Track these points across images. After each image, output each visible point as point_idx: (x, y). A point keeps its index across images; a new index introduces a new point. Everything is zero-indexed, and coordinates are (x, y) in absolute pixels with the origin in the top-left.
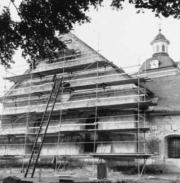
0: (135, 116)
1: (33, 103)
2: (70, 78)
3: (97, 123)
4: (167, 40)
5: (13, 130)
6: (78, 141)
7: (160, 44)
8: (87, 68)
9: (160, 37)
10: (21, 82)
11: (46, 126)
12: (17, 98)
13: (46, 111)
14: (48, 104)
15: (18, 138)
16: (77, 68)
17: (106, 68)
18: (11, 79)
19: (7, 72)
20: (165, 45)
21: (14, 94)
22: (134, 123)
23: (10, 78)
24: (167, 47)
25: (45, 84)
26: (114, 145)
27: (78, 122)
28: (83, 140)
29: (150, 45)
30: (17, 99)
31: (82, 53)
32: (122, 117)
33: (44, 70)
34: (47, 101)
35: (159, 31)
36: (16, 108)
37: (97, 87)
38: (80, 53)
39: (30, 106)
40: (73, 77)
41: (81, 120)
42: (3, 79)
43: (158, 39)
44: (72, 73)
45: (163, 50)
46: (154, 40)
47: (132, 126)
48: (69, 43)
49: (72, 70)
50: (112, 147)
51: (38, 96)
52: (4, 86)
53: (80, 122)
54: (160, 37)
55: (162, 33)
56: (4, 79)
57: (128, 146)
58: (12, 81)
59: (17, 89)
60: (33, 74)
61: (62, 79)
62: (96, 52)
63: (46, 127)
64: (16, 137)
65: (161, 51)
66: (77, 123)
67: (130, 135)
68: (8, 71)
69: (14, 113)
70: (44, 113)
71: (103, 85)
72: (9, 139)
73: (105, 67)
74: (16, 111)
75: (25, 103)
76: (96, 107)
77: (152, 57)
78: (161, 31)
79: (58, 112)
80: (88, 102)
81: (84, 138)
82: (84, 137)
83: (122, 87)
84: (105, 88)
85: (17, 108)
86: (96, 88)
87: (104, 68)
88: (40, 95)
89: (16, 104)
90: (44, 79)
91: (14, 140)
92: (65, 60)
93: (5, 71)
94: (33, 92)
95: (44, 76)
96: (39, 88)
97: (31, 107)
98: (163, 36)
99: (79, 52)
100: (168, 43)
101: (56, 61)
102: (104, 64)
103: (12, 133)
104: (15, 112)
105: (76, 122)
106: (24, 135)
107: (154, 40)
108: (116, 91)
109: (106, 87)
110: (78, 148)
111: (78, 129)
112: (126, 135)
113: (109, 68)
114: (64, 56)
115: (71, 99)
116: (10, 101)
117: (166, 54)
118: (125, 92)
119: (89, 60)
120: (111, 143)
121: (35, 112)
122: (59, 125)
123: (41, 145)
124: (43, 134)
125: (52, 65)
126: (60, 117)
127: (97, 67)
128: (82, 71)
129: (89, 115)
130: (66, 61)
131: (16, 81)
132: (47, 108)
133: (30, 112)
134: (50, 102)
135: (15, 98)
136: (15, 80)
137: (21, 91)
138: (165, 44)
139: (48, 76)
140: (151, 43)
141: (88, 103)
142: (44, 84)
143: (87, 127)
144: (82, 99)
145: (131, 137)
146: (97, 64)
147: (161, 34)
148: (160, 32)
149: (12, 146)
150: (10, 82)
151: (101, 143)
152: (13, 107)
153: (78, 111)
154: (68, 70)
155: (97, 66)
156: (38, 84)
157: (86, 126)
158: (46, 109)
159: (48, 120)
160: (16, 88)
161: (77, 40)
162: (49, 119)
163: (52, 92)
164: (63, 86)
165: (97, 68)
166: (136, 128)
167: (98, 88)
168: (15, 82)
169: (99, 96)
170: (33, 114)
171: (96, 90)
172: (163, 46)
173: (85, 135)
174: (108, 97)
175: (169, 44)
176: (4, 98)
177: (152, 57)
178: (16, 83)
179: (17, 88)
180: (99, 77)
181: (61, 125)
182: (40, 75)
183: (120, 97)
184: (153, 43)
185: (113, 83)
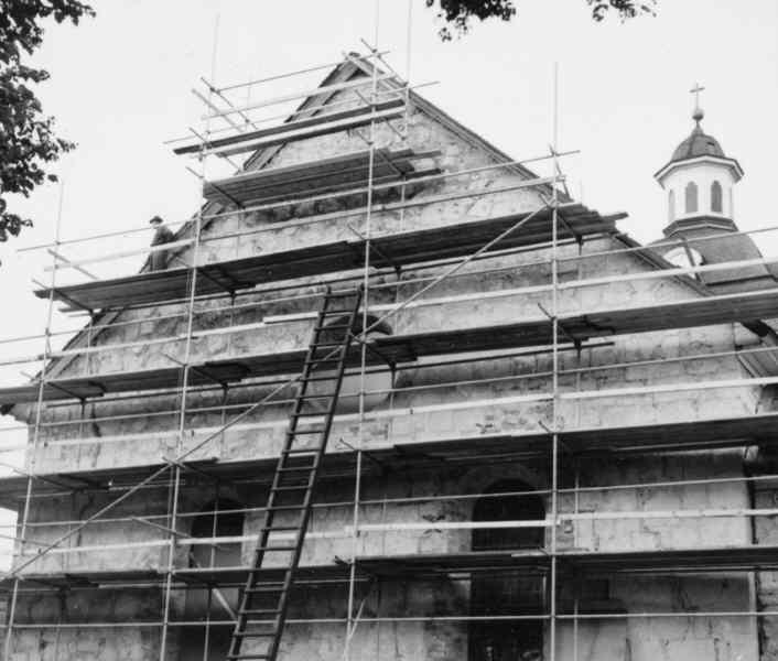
0: (744, 486)
1: (200, 413)
2: (388, 294)
3: (565, 517)
4: (736, 161)
5: (80, 553)
7: (703, 176)
9: (698, 148)
10: (120, 312)
11: (295, 529)
12: (105, 390)
13: (286, 454)
14: (296, 418)
17: (586, 244)
18: (74, 297)
20: (722, 184)
22: (744, 519)
24: (731, 190)
25: (266, 319)
27: (435, 514)
28: (460, 608)
29: (655, 180)
31: (447, 171)
32: (679, 491)
33: (247, 252)
35: (694, 122)
36: (93, 440)
37: (555, 337)
38: (437, 171)
40: (425, 284)
41: (450, 502)
43: (690, 156)
44: (398, 271)
46: (674, 161)
47: (738, 538)
49: (405, 251)
51: (219, 385)
53: (448, 516)
54: (698, 148)
55: (708, 128)
56: (42, 294)
57: (717, 640)
58: (77, 306)
59: (99, 348)
60: (200, 270)
62: (519, 165)
64: (101, 587)
65: (704, 209)
66: (430, 519)
68: (62, 259)
69: (86, 465)
72: (62, 598)
73: (580, 241)
74: (99, 457)
75: (152, 418)
76: (555, 438)
77: (662, 236)
78: (701, 123)
79: (346, 460)
80: (490, 413)
81: (468, 595)
82: (468, 589)
83: (671, 338)
84: (584, 343)
87: (576, 246)
89: (97, 420)
90: (247, 300)
91: (92, 604)
92: (374, 201)
95: (252, 285)
96: (219, 344)
97: (193, 433)
98: (712, 143)
99: (431, 168)
100: (736, 172)
101: (288, 215)
102: (578, 223)
103: (77, 567)
104: (94, 465)
105: (424, 517)
108: (639, 355)
109: (586, 339)
111: (439, 547)
113: (595, 246)
114: (367, 185)
115: (396, 397)
116: (67, 408)
117: (728, 222)
118: (688, 363)
119: (484, 208)
122: (349, 529)
124: (246, 573)
126: (752, 481)
128: (467, 258)
129: (492, 481)
130: (379, 207)
131: (97, 311)
133: (189, 459)
134: (302, 412)
135: (96, 390)
136: (92, 303)
137: (117, 359)
138: (723, 177)
139: (267, 286)
140: (656, 176)
141: (489, 418)
142: (261, 320)
143: (479, 538)
144: (451, 402)
145: (733, 593)
147: (703, 135)
148: (698, 126)
150: (64, 311)
151: (572, 620)
152: (85, 436)
154: (392, 253)
155: (551, 230)
157: (475, 532)
158: (289, 444)
161: (421, 111)
163: (312, 358)
165: (554, 242)
166: (751, 546)
167: (367, 365)
168: (91, 311)
169: (194, 420)
170: (202, 474)
172: (716, 188)
173: (469, 582)
175: (740, 182)
177: (662, 236)
178: (96, 319)
179: (103, 343)
180: (562, 286)
181: (364, 527)
184: (666, 175)
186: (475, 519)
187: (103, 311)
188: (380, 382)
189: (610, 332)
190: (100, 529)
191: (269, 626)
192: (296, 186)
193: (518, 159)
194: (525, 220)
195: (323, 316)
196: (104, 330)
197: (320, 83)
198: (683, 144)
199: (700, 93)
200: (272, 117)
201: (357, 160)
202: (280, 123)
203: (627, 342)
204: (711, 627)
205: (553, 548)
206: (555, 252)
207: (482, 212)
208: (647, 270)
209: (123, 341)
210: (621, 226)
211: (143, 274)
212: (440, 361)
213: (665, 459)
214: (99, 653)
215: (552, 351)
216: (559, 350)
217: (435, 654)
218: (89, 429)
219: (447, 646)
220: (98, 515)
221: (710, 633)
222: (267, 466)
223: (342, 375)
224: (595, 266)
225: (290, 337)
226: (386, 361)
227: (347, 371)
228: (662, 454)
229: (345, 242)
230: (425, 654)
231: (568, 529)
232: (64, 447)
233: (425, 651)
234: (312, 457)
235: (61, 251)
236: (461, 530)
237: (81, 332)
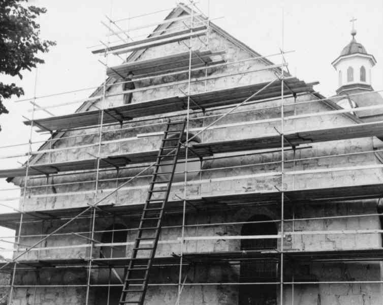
0: (378, 219)
1: (105, 182)
2: (199, 123)
3: (288, 233)
6: (225, 279)
7: (356, 64)
8: (252, 96)
9: (354, 50)
10: (66, 132)
13: (148, 202)
14: (153, 184)
15: (60, 270)
16: (208, 98)
18: (42, 125)
19: (35, 107)
20: (365, 66)
21: (48, 162)
23: (41, 120)
25: (138, 135)
26: (324, 291)
29: (332, 66)
30: (59, 173)
34: (151, 177)
35: (352, 36)
36: (53, 195)
37: (283, 144)
38: (223, 61)
39: (100, 191)
42: (23, 124)
43: (349, 53)
44: (204, 112)
45: (363, 78)
46: (340, 57)
48: (198, 36)
49: (207, 102)
50: (319, 295)
51: (115, 168)
52: (28, 142)
53: (229, 233)
54: (354, 50)
55: (358, 39)
56: (27, 123)
59: (55, 150)
60: (105, 110)
61: (185, 123)
62: (264, 58)
63: (133, 243)
64: (57, 267)
67: (368, 267)
70: (145, 207)
71: (294, 140)
75: (82, 185)
77: (336, 94)
78: (355, 37)
79: (178, 205)
80: (250, 182)
83: (340, 145)
84: (297, 147)
85: (57, 195)
86: (281, 146)
88: (121, 165)
89: (54, 185)
93: (31, 104)
94: (105, 155)
96: (115, 148)
100: (373, 61)
101: (160, 82)
102: (294, 87)
103: (45, 258)
104: (53, 207)
105: (217, 233)
106: (82, 262)
107: (343, 56)
108: (325, 153)
109: (298, 145)
110: (213, 295)
111: (224, 248)
112: (361, 267)
113: (303, 98)
116: (38, 179)
118: (350, 156)
120: (317, 285)
121: (113, 205)
122: (180, 239)
123: (143, 287)
125: (148, 92)
127: (281, 95)
129: (250, 216)
130: (194, 79)
131: (54, 131)
132: (151, 194)
133: (100, 204)
136: (52, 128)
138: (366, 64)
139: (138, 119)
140: (332, 64)
142: (136, 136)
143: (244, 244)
146: (281, 88)
148: (354, 38)
149: (46, 289)
150: (38, 131)
151: (291, 285)
152: (48, 193)
153: (225, 204)
154: (202, 103)
155: (281, 90)
156: (113, 136)
157: (242, 241)
159: (159, 223)
160: (53, 148)
161: (215, 31)
162: (159, 221)
164: (187, 140)
168: (51, 132)
170: (105, 211)
171: (185, 162)
172: (363, 70)
173: (239, 266)
174: (304, 169)
175: (374, 67)
176: (29, 170)
178: (54, 135)
179: (57, 147)
181: (187, 238)
182: (121, 114)
183: (337, 169)
184: (338, 63)
185: (323, 134)
186: (242, 235)
187: (57, 131)
188: (195, 166)
189: (310, 141)
190: (56, 238)
191: (140, 287)
192: (152, 69)
193: (263, 55)
194: (268, 85)
195: (166, 134)
196: (58, 141)
197: (165, 18)
198: (346, 47)
199: (355, 22)
200: (141, 35)
201: (183, 56)
202: (145, 38)
203: (318, 146)
204: (203, 294)
205: (282, 249)
206: (284, 102)
207: (246, 82)
208: (328, 110)
209: (67, 146)
210: (316, 88)
211: (77, 113)
212: (224, 156)
213: (338, 204)
214: (56, 299)
215: (281, 151)
216: (284, 150)
217: (222, 301)
218: (51, 190)
219: (228, 297)
220: (55, 231)
221: (361, 291)
222: (139, 208)
223: (176, 163)
224: (303, 108)
225: (151, 144)
226: (198, 156)
227: (178, 161)
228: (356, 201)
229: (177, 97)
230: (217, 301)
231: (289, 239)
232: (38, 198)
233: (218, 299)
234: (162, 203)
235: (36, 101)
236: (235, 240)
237: (46, 142)
